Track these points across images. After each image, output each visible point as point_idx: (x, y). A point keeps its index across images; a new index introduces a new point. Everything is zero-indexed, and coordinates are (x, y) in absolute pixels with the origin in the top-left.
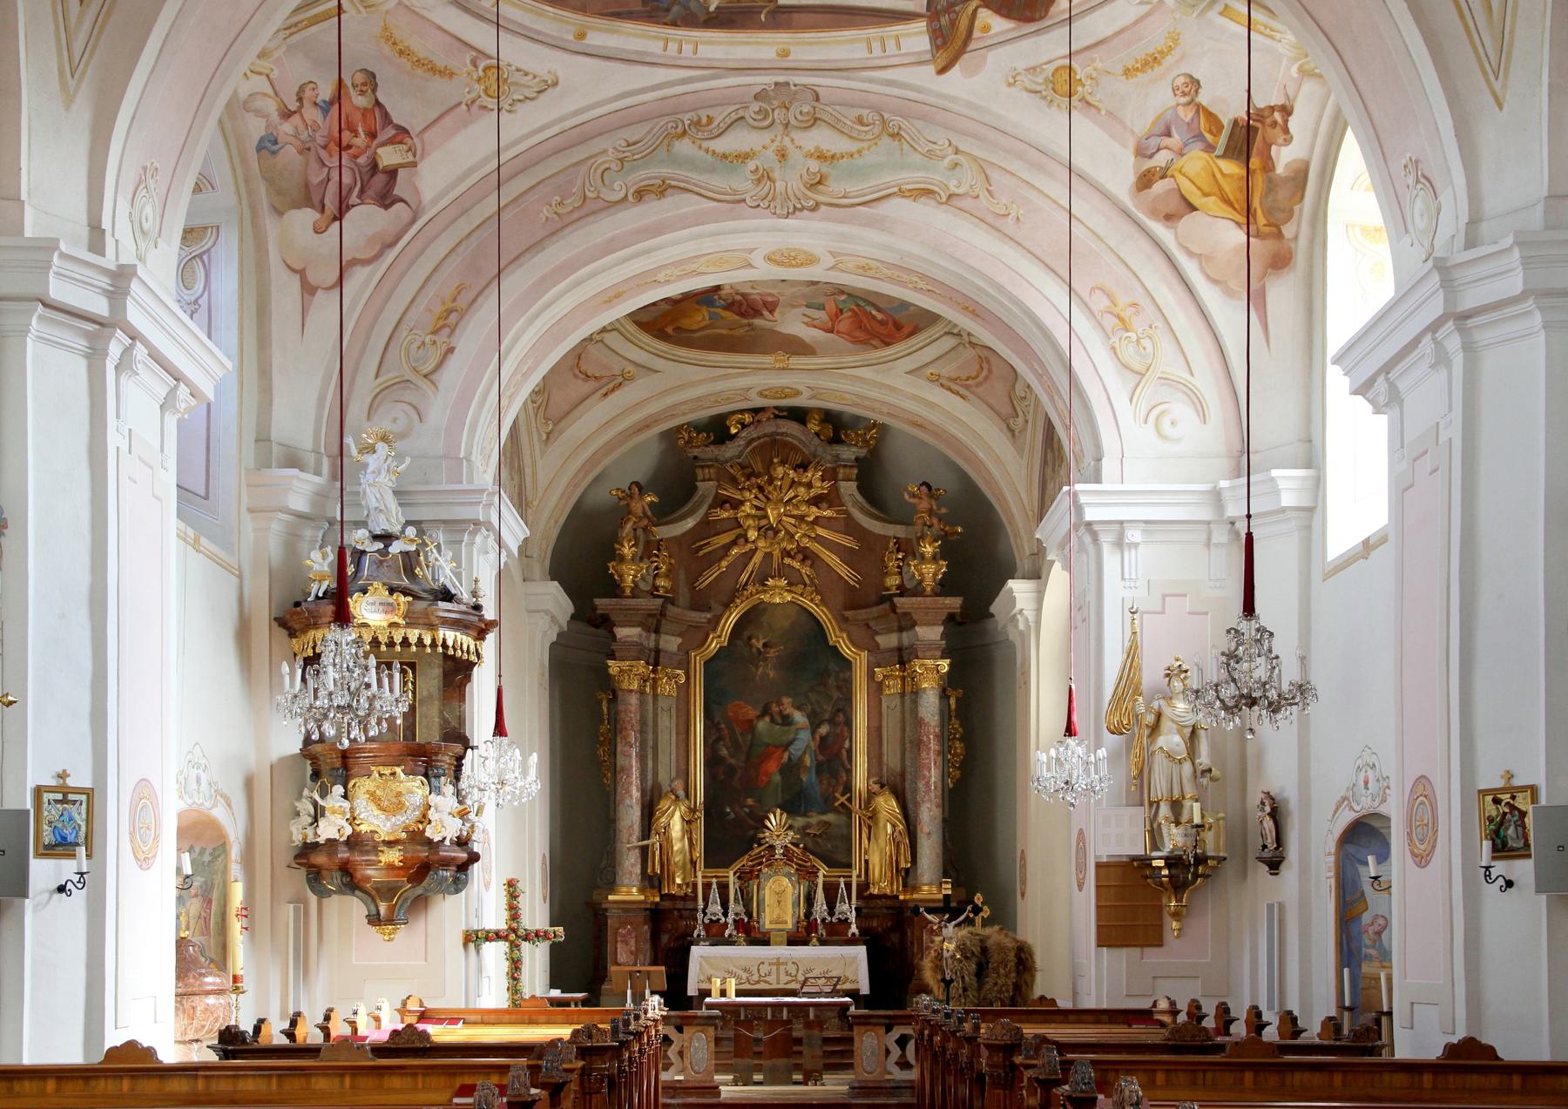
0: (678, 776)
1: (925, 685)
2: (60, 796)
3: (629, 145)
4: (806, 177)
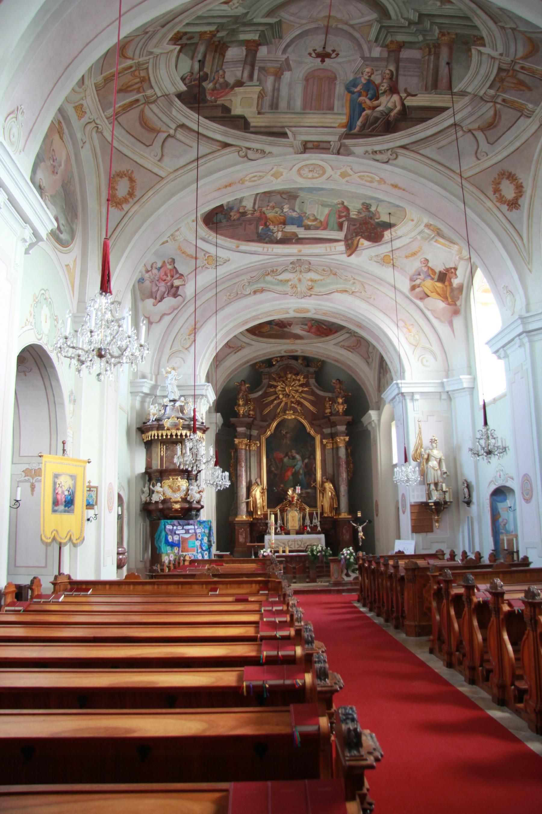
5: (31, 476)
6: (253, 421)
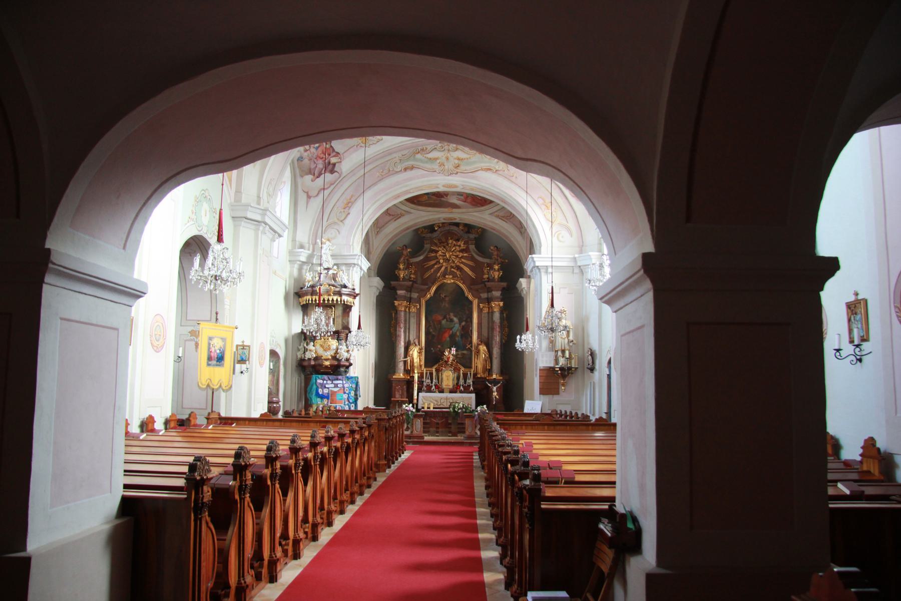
0: (416, 338)
1: (495, 310)
2: (242, 347)
3: (403, 156)
4: (454, 165)
5: (195, 336)
6: (412, 285)
